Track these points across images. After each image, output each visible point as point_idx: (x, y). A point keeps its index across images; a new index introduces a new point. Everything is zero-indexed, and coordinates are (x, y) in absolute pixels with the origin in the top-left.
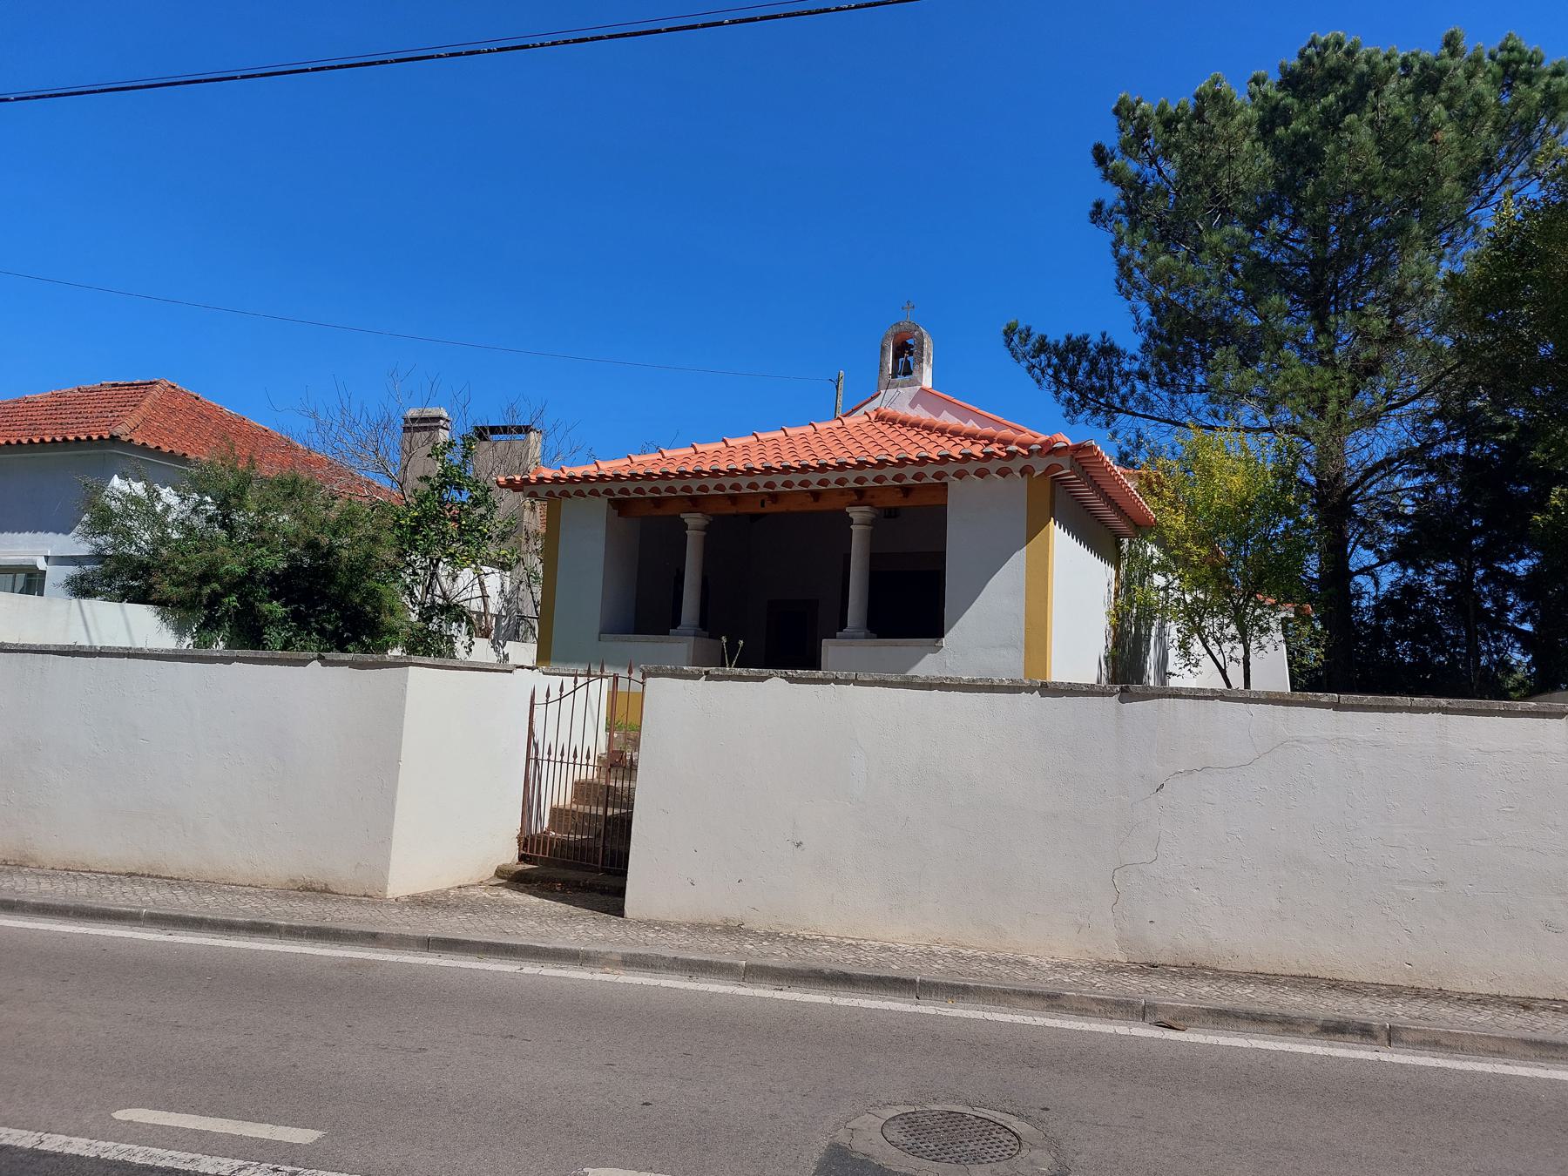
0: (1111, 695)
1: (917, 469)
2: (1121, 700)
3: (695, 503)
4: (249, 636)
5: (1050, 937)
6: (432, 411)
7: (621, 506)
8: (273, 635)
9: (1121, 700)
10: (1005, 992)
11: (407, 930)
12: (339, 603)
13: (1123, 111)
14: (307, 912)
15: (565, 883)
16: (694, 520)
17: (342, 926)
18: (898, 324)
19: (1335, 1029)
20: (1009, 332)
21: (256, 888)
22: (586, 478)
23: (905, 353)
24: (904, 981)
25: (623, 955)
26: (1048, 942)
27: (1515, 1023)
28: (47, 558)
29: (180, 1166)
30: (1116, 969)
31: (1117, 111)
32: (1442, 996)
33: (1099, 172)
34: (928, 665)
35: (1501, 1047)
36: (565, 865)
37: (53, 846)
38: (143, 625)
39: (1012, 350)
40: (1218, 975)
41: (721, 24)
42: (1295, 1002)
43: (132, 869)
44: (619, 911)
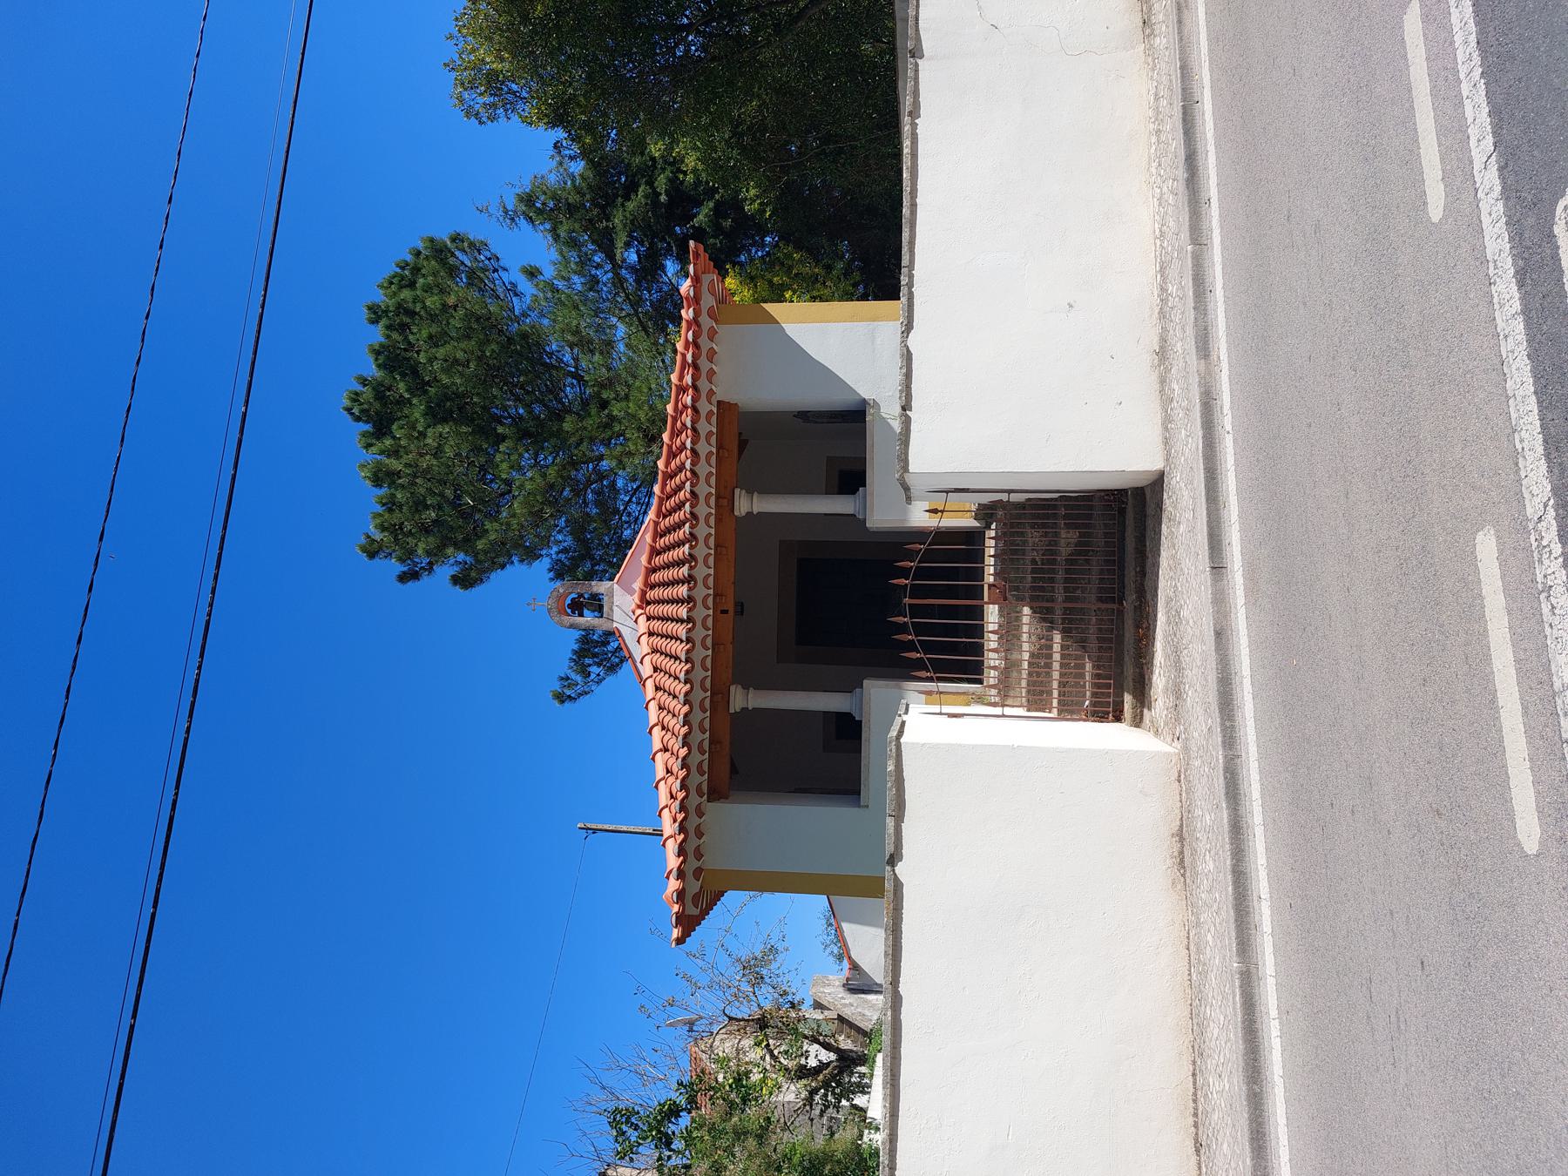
0: (917, 65)
1: (693, 792)
2: (922, 57)
3: (719, 695)
9: (922, 57)
10: (1181, 39)
11: (1206, 594)
14: (1212, 862)
15: (1138, 626)
16: (740, 699)
17: (1212, 677)
18: (549, 611)
20: (561, 698)
21: (1192, 946)
22: (681, 852)
24: (1185, 114)
25: (1199, 359)
26: (1131, 97)
29: (1473, 38)
30: (1150, 51)
33: (426, 579)
34: (889, 410)
36: (1120, 662)
39: (580, 695)
41: (245, 414)
43: (1190, 1143)
44: (1158, 482)
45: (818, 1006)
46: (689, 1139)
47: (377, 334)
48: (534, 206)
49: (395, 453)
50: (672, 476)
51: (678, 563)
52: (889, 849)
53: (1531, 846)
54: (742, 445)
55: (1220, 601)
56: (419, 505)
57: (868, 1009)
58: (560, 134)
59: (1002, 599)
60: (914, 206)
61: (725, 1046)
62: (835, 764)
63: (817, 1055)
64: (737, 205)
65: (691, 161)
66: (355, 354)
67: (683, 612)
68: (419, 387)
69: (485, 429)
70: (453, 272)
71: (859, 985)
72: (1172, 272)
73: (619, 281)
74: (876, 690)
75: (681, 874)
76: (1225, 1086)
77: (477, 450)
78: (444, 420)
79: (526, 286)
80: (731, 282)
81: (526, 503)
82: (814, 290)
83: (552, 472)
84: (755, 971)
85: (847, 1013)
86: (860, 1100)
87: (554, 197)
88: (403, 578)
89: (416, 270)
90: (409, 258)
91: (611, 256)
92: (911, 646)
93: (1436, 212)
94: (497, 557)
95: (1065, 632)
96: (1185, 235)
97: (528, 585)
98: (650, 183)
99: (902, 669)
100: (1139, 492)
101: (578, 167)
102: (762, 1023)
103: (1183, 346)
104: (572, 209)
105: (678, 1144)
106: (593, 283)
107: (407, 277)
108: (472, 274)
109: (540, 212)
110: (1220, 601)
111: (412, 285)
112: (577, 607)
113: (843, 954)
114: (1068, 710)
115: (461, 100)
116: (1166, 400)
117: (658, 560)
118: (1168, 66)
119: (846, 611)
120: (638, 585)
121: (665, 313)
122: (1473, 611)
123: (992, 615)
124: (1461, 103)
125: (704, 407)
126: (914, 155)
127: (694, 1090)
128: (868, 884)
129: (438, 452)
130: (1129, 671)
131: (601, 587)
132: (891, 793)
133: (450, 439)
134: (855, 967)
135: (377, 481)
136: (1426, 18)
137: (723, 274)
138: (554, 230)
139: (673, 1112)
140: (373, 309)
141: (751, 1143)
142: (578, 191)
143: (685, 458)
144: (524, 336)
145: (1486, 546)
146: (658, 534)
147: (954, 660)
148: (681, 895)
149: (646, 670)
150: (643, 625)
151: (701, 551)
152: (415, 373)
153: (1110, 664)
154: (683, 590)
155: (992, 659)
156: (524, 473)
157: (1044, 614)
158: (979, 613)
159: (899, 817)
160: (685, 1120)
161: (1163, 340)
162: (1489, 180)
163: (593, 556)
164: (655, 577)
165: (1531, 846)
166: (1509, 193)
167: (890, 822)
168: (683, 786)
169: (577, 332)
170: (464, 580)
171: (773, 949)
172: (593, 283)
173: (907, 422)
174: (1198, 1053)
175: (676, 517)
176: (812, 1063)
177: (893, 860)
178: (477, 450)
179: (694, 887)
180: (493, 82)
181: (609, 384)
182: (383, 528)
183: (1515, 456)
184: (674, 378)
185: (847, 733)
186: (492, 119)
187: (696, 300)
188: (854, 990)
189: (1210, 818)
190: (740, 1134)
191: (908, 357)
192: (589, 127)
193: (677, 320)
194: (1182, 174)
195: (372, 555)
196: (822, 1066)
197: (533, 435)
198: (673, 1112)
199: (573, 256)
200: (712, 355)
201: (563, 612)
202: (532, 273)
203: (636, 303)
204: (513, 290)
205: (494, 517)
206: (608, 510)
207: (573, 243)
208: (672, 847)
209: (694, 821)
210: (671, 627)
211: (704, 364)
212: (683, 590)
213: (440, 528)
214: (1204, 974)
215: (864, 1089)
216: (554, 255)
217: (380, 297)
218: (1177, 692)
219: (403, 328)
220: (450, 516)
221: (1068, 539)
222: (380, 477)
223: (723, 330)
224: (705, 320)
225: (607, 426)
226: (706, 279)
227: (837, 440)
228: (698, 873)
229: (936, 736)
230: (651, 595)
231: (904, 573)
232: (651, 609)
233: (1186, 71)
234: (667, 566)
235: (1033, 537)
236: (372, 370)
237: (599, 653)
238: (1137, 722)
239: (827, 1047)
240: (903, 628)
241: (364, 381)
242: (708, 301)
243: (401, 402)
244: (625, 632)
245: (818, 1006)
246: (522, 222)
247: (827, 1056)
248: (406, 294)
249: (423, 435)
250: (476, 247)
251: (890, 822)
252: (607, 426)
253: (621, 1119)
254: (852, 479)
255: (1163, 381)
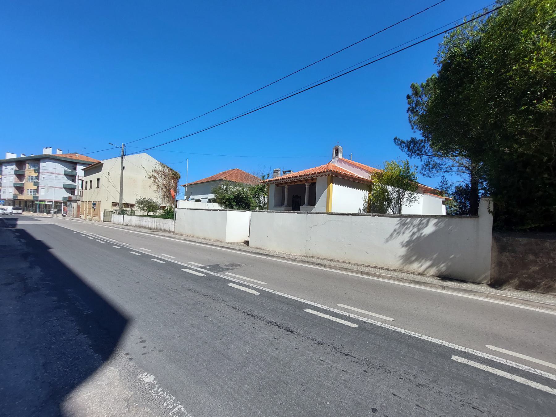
4: (232, 207)
5: (296, 251)
6: (277, 169)
7: (277, 185)
12: (244, 203)
13: (413, 86)
19: (318, 264)
23: (337, 151)
27: (358, 268)
32: (349, 263)
38: (216, 206)
40: (318, 258)
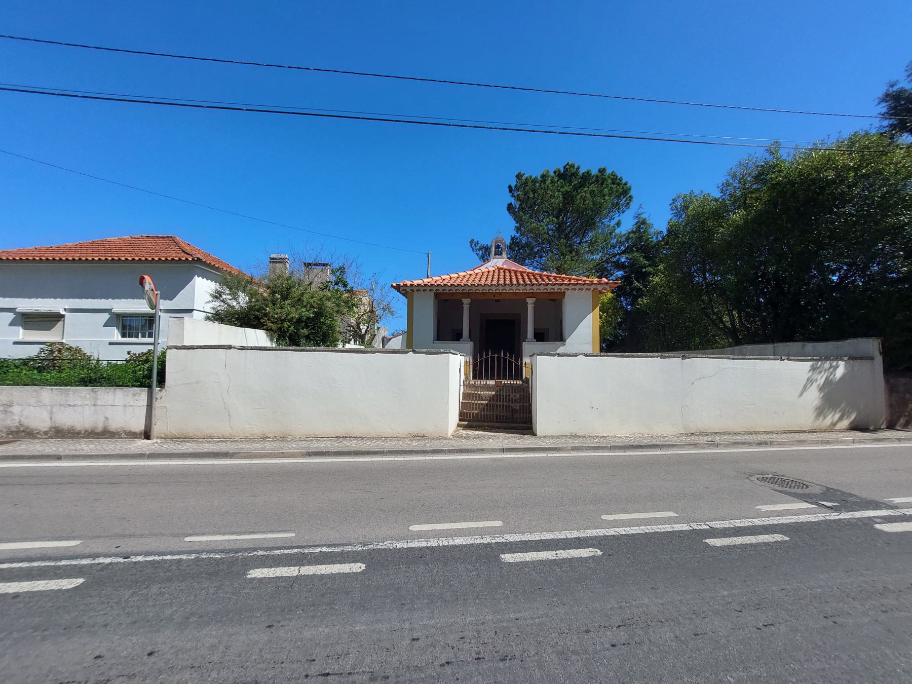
3: (467, 295)
8: (303, 341)
14: (415, 445)
16: (466, 301)
17: (469, 447)
19: (760, 444)
20: (472, 242)
21: (392, 438)
22: (419, 285)
26: (666, 429)
28: (65, 309)
30: (682, 435)
31: (517, 176)
33: (509, 194)
34: (561, 350)
35: (793, 443)
36: (478, 421)
37: (299, 428)
38: (259, 337)
42: (748, 438)
44: (533, 434)
45: (379, 328)
46: (337, 291)
47: (595, 172)
48: (642, 224)
49: (552, 182)
50: (541, 277)
51: (517, 280)
52: (417, 350)
53: (411, 528)
54: (553, 300)
55: (493, 451)
56: (534, 191)
57: (378, 344)
58: (665, 233)
59: (497, 385)
60: (629, 357)
61: (366, 300)
62: (447, 333)
63: (363, 328)
64: (641, 296)
65: (657, 279)
66: (588, 164)
67: (508, 282)
68: (576, 188)
69: (560, 212)
70: (618, 197)
71: (385, 341)
72: (602, 440)
73: (615, 255)
74: (469, 346)
75: (412, 285)
76: (353, 445)
77: (553, 210)
78: (564, 197)
79: (613, 223)
80: (610, 295)
81: (535, 228)
82: (598, 322)
83: (546, 236)
84: (387, 308)
85: (377, 337)
86: (352, 342)
87: (644, 232)
88: (510, 187)
89: (619, 184)
90: (624, 181)
91: (623, 253)
92: (481, 357)
93: (604, 517)
94: (518, 219)
95: (487, 404)
96: (614, 444)
97: (507, 229)
98: (649, 265)
99: (477, 353)
100: (531, 428)
101: (654, 239)
102: (372, 311)
103: (577, 443)
104: (640, 238)
105: (336, 287)
106: (613, 247)
107: (616, 181)
108: (617, 204)
109: (639, 227)
110: (493, 451)
111: (613, 183)
112: (498, 247)
113: (394, 336)
114: (463, 405)
115: (679, 197)
116: (559, 437)
117: (513, 273)
118: (675, 440)
119: (496, 336)
120: (505, 267)
121: (602, 271)
122: (478, 519)
123: (492, 383)
124: (638, 526)
125: (563, 287)
126: (647, 357)
127: (351, 291)
128: (411, 345)
129: (552, 196)
130: (475, 424)
131: (504, 255)
132: (434, 350)
133: (557, 199)
134: (390, 339)
135: (543, 176)
136: (670, 518)
137: (613, 292)
138: (633, 232)
139: (345, 285)
140: (604, 170)
141: (336, 309)
142: (648, 239)
143: (560, 281)
144: (594, 224)
145: (498, 523)
146: (521, 273)
147: (479, 370)
148: (406, 285)
149: (477, 271)
150: (491, 269)
151: (528, 288)
152: (580, 187)
153: (476, 418)
154: (508, 282)
155: (478, 382)
156: (547, 225)
157: (492, 398)
158: (492, 378)
159: (426, 353)
160: (343, 289)
161: (580, 437)
162: (611, 532)
163: (518, 251)
164: (507, 273)
165: (411, 528)
166: (606, 537)
167: (425, 350)
168: (438, 285)
169: (596, 242)
170: (510, 207)
171: (393, 314)
172: (613, 247)
173: (554, 355)
174: (362, 438)
175: (540, 280)
176: (361, 327)
177: (414, 351)
178: (553, 210)
179: (408, 290)
180: (686, 208)
181: (577, 253)
182: (526, 179)
183: (523, 533)
184: (574, 277)
185: (457, 336)
186: (672, 209)
187: (600, 284)
188: (383, 339)
189: (428, 445)
190: (338, 305)
191: (576, 355)
192: (667, 243)
193: (600, 277)
194: (636, 444)
195: (517, 176)
196: (360, 330)
197: (560, 228)
198: (345, 285)
199: (623, 239)
200: (581, 289)
201: (496, 242)
202: (618, 224)
203: (607, 262)
204: (612, 218)
205: (531, 217)
206: (532, 255)
207: (628, 239)
208: (420, 282)
209: (428, 289)
210: (490, 278)
211: (578, 287)
212: (515, 282)
213: (527, 198)
214: (384, 441)
215: (355, 343)
216: (624, 232)
217: (609, 172)
218: (466, 437)
219: (597, 181)
220: (531, 202)
221: (517, 406)
222: (544, 177)
223: (590, 293)
224: (592, 287)
225: (563, 254)
226: (607, 287)
227: (552, 332)
228: (412, 290)
229: (455, 365)
230: (502, 271)
231: (505, 355)
232: (497, 271)
233: (672, 446)
234: (511, 277)
235: (518, 396)
236: (582, 171)
237: (485, 254)
238: (459, 426)
239: (366, 331)
240: (487, 354)
241: (578, 168)
242: (600, 288)
243: (570, 182)
244: (489, 264)
245: (379, 328)
246: (636, 221)
247: (363, 331)
248: (610, 181)
249: (559, 191)
250: (627, 205)
251: (425, 350)
252: (563, 254)
253: (342, 270)
254: (540, 337)
255: (566, 436)
